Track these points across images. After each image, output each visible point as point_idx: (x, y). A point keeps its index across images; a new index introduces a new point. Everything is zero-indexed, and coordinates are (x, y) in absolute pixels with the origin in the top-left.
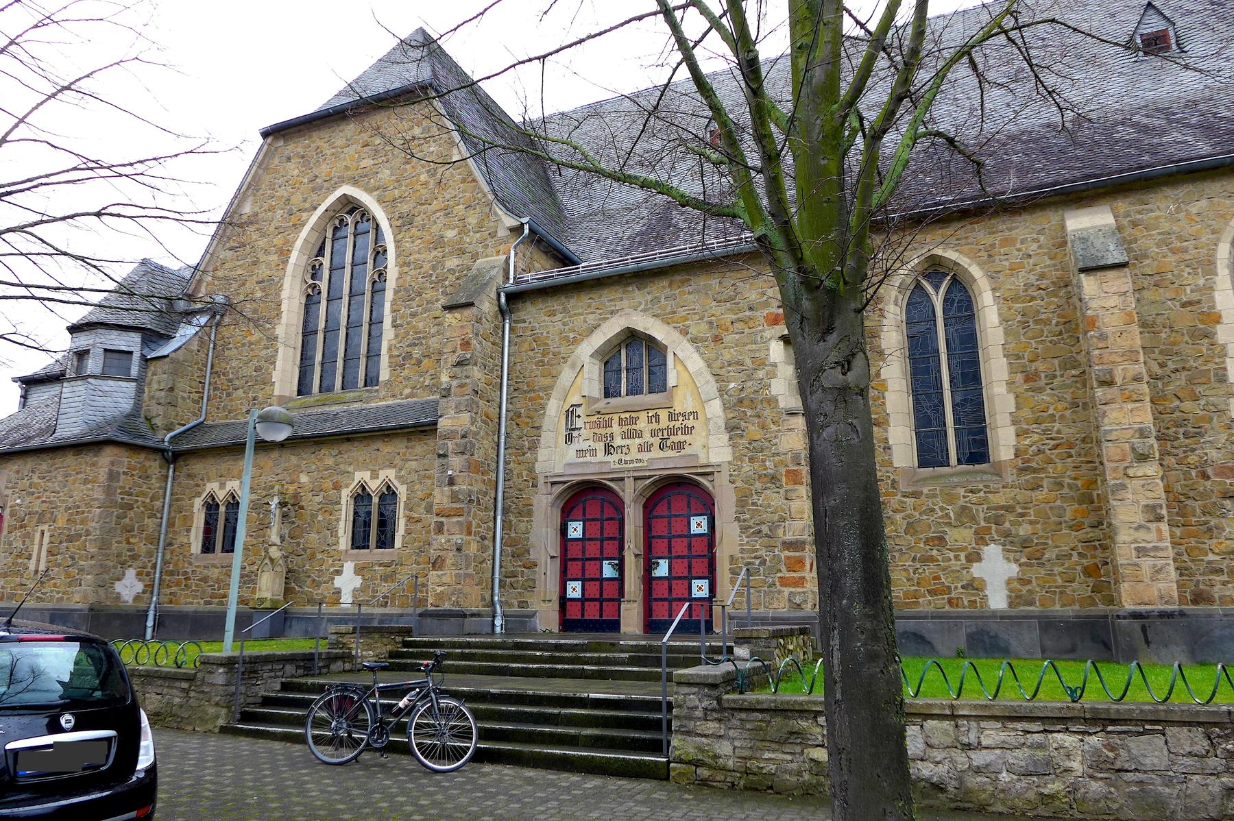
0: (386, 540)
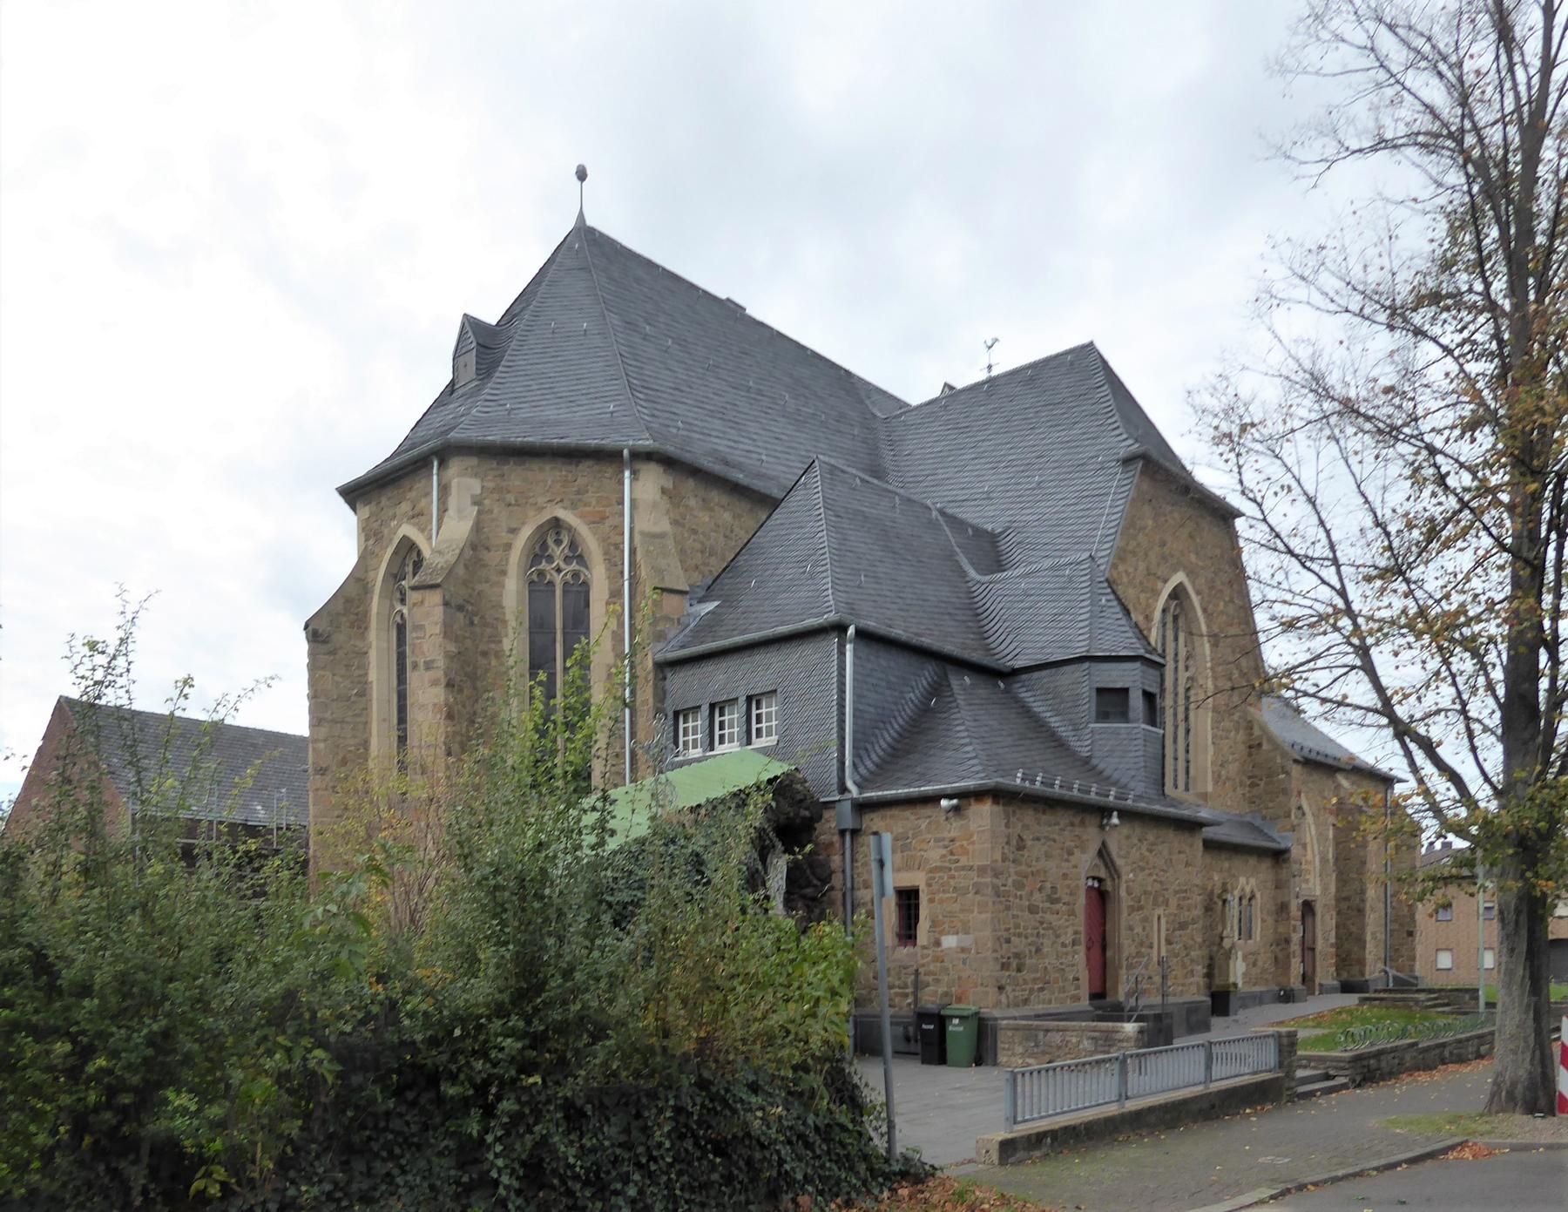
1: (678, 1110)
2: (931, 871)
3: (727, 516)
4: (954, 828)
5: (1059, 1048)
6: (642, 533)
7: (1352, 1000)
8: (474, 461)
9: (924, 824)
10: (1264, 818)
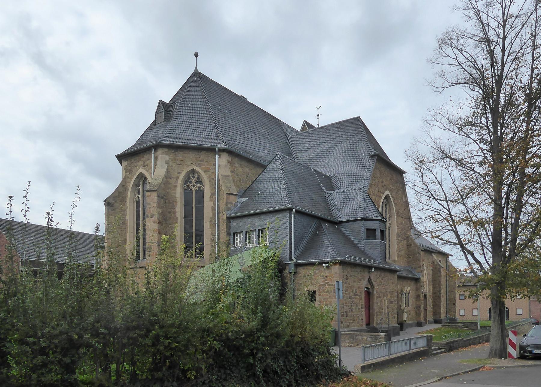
1: (298, 356)
2: (319, 286)
3: (247, 170)
4: (327, 273)
5: (360, 340)
6: (222, 175)
7: (439, 326)
8: (166, 150)
9: (317, 271)
10: (412, 268)
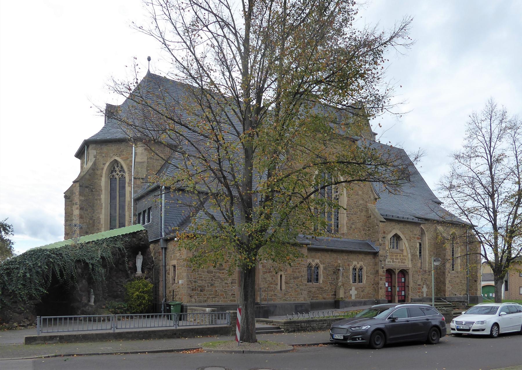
0: (360, 281)
6: (137, 162)
8: (94, 145)
10: (372, 241)
